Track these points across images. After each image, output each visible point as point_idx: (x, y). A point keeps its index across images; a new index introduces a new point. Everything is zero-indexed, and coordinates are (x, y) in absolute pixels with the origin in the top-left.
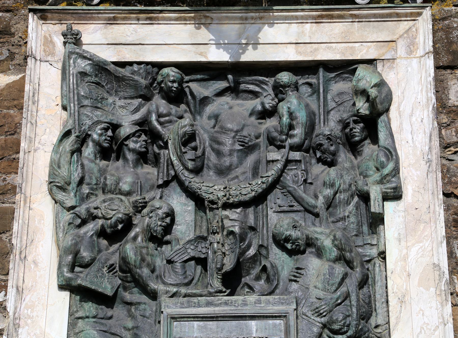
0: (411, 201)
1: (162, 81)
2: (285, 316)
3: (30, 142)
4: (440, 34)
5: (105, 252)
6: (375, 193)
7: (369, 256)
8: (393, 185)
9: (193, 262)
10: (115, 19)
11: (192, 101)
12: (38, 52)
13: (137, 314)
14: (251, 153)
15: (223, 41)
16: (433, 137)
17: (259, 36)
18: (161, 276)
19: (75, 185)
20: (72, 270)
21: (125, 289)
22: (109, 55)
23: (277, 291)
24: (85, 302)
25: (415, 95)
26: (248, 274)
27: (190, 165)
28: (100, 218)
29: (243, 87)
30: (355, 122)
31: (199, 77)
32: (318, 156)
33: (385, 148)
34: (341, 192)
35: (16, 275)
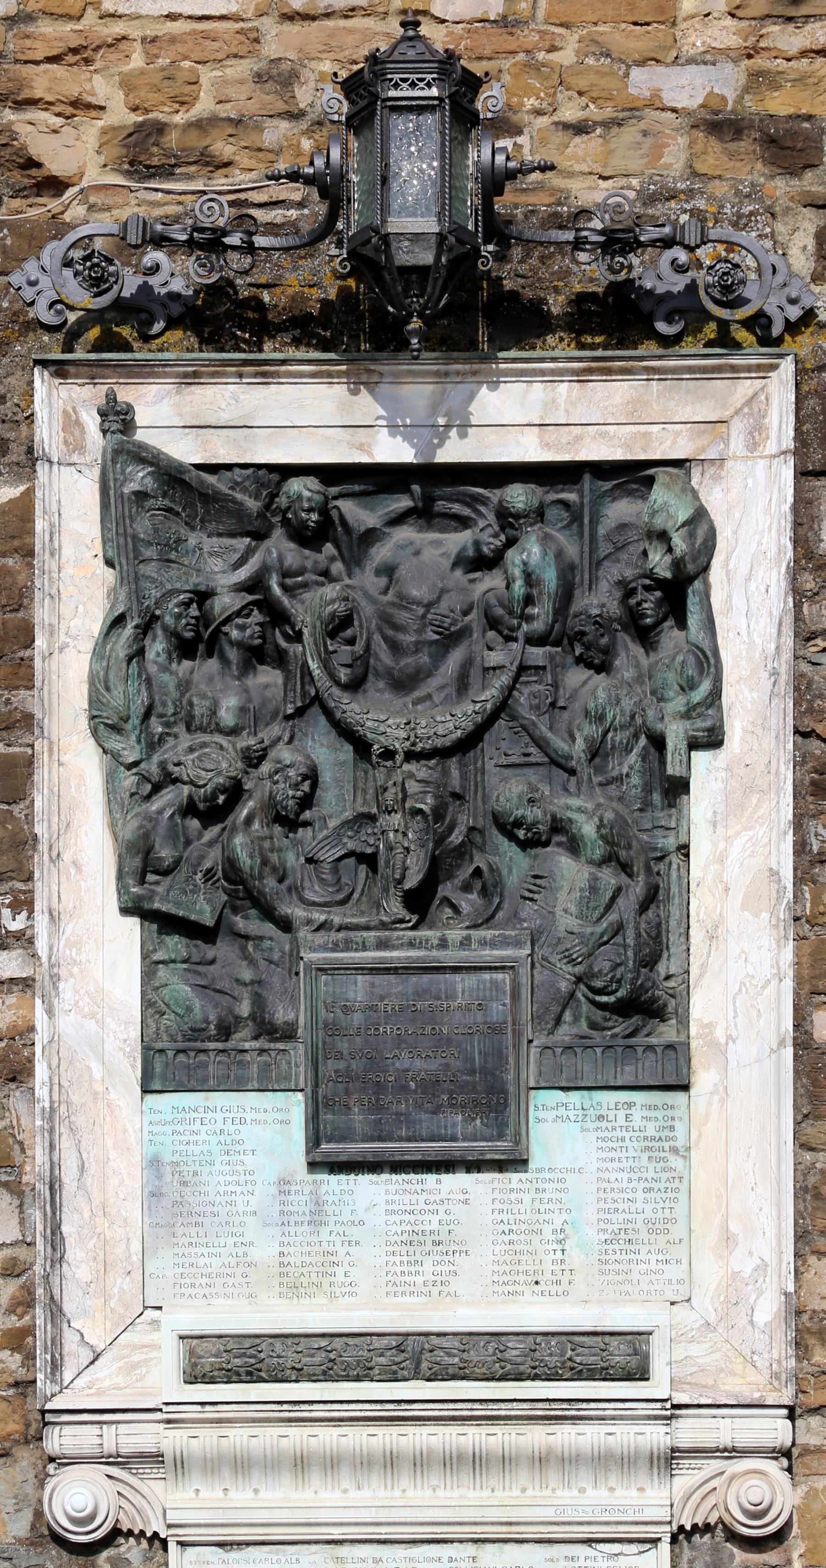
0: (738, 751)
1: (289, 508)
2: (512, 967)
3: (51, 634)
4: (812, 402)
5: (196, 844)
6: (675, 734)
7: (662, 850)
8: (708, 723)
9: (351, 861)
10: (195, 374)
11: (345, 538)
12: (54, 447)
13: (258, 956)
14: (456, 645)
15: (403, 420)
16: (783, 629)
17: (470, 409)
18: (296, 888)
19: (137, 722)
20: (142, 881)
21: (235, 910)
22: (185, 451)
23: (500, 915)
24: (168, 934)
25: (757, 537)
26: (450, 876)
27: (343, 675)
28: (185, 783)
29: (441, 506)
30: (647, 588)
31: (357, 488)
32: (577, 653)
33: (698, 647)
34: (615, 730)
35: (46, 889)
